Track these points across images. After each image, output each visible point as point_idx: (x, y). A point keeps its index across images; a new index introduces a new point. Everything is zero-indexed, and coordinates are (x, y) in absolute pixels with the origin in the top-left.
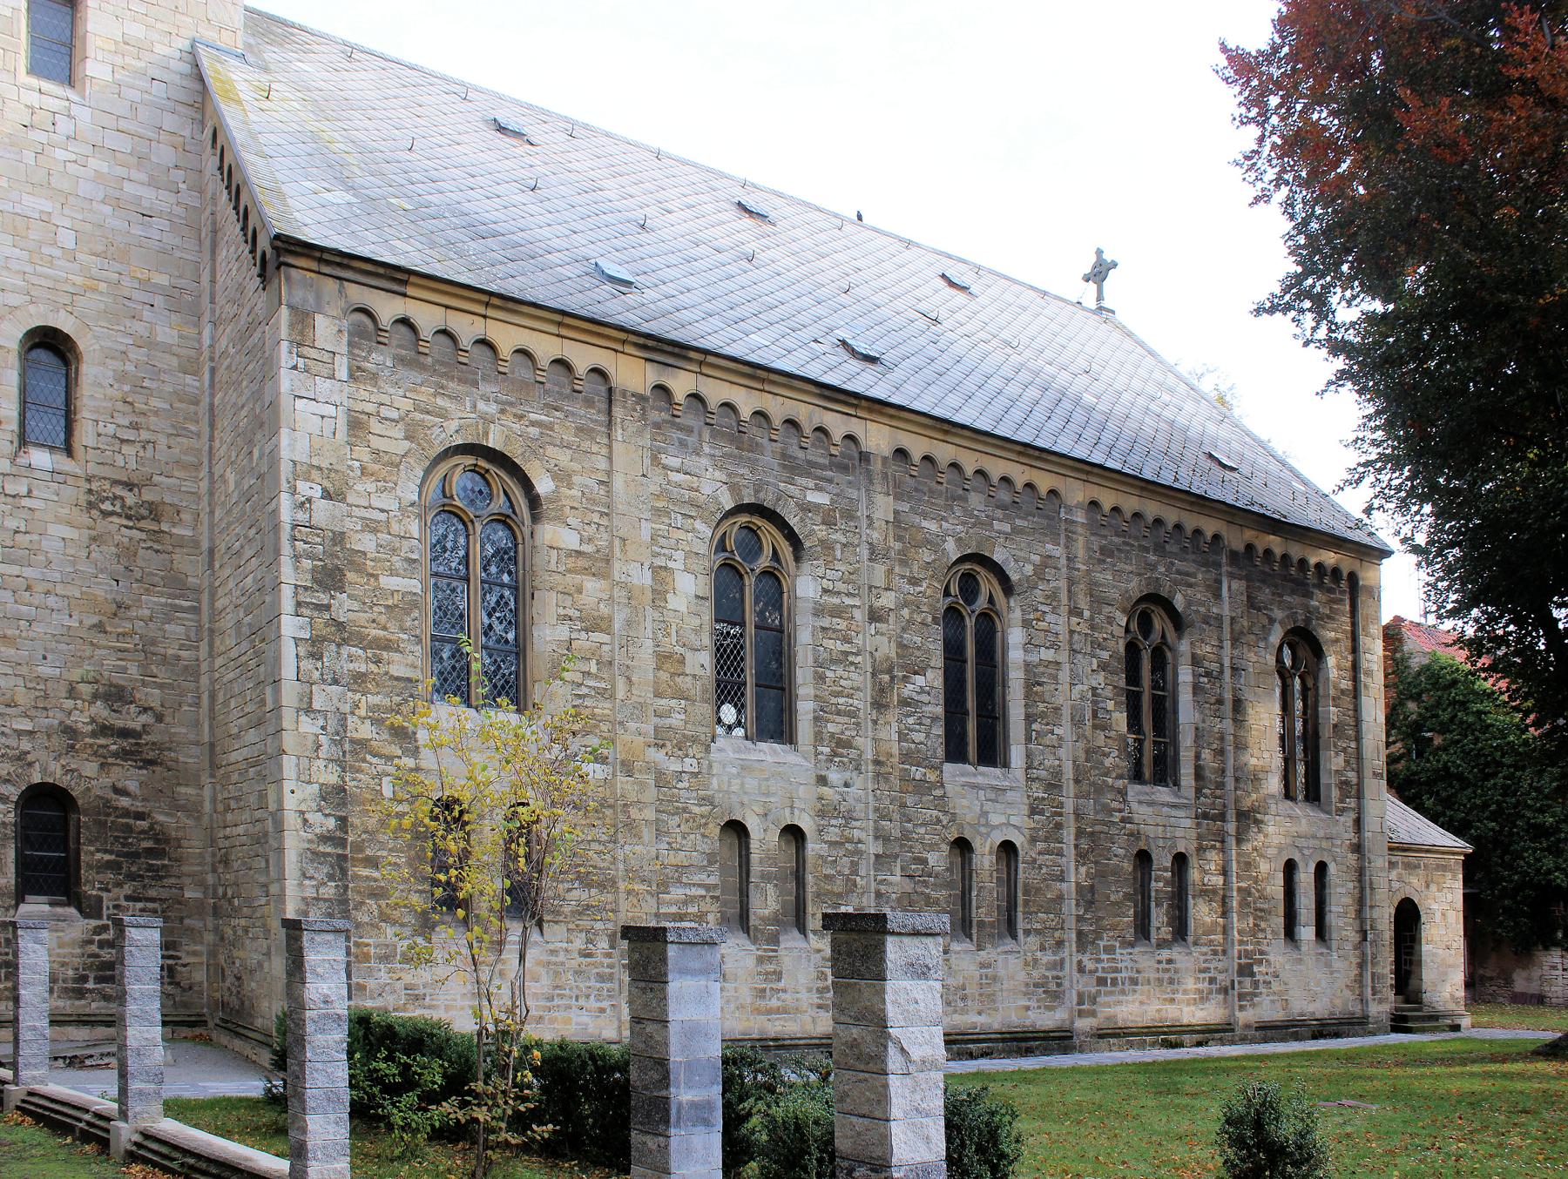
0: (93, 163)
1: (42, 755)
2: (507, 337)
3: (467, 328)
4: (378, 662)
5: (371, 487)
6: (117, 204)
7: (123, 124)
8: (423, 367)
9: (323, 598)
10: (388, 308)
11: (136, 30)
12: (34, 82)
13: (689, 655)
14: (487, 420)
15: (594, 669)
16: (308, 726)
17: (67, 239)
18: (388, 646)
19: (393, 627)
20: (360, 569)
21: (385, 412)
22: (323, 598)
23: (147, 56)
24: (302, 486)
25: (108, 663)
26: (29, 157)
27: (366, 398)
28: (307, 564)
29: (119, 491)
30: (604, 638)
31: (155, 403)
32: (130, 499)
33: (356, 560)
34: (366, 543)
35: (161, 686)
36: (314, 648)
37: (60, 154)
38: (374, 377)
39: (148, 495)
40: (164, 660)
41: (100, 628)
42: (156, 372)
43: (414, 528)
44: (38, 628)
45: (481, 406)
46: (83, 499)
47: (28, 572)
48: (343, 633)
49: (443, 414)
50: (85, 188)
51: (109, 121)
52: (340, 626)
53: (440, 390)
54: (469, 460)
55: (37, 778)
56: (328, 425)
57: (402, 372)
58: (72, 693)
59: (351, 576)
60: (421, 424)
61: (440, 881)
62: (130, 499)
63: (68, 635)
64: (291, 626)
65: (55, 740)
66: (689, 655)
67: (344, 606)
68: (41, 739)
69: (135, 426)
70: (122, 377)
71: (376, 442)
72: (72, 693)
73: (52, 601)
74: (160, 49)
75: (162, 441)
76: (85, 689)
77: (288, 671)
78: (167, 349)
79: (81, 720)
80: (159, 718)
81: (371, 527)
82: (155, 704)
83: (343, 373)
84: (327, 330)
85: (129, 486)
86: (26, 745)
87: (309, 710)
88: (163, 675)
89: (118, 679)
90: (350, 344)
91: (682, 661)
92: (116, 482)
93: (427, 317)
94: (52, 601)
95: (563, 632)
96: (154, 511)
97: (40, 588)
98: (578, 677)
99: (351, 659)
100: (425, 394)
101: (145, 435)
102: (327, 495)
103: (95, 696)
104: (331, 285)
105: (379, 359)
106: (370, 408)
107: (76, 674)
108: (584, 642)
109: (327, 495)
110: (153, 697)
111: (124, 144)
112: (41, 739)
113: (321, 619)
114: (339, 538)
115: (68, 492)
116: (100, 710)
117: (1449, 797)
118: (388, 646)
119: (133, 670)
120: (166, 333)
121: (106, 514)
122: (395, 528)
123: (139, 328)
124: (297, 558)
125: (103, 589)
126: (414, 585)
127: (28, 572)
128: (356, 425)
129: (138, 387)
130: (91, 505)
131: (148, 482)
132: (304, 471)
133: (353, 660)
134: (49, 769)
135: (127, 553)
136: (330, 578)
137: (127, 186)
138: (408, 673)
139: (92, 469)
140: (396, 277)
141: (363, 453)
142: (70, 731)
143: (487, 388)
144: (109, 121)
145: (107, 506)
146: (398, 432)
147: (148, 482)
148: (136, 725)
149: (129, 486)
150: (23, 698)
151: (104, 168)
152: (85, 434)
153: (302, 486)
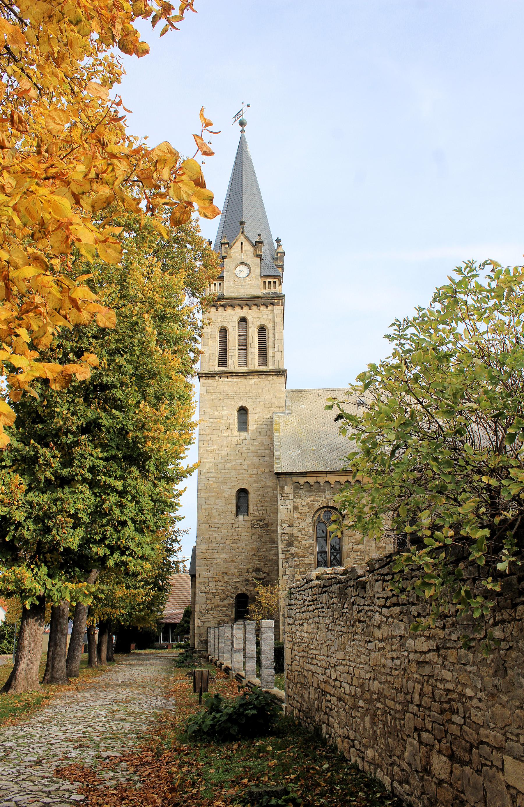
0: (251, 448)
1: (241, 586)
2: (332, 479)
3: (322, 480)
4: (302, 561)
5: (300, 521)
6: (257, 456)
7: (258, 437)
8: (312, 491)
9: (288, 549)
10: (302, 480)
11: (260, 415)
12: (239, 433)
13: (387, 546)
14: (328, 500)
15: (359, 553)
16: (285, 578)
17: (246, 467)
18: (305, 557)
19: (306, 552)
20: (297, 540)
21: (303, 504)
22: (288, 549)
23: (263, 420)
24: (283, 525)
25: (257, 563)
26: (237, 451)
27: (298, 502)
28: (285, 542)
29: (258, 522)
30: (362, 545)
31: (267, 500)
32: (261, 523)
33: (296, 539)
34: (299, 534)
35: (269, 567)
36: (286, 560)
37: (244, 449)
38: (300, 496)
39: (265, 522)
40: (269, 560)
41: (254, 555)
42: (266, 492)
43: (311, 528)
44: (240, 557)
45: (327, 497)
46: (250, 526)
47: (238, 545)
48: (293, 556)
49: (317, 501)
50: (249, 455)
51: (255, 438)
52: (292, 554)
53: (316, 495)
54: (325, 509)
55: (240, 592)
56: (289, 510)
57: (307, 493)
58: (248, 571)
59: (295, 542)
60: (312, 504)
61: (494, 581)
62: (261, 523)
63: (247, 558)
64: (281, 556)
65: (244, 583)
66: (387, 546)
67: (293, 550)
68: (241, 583)
69: (262, 506)
70: (258, 496)
71: (301, 511)
72: (248, 571)
73: (243, 550)
74: (265, 418)
75: (268, 508)
76: (251, 570)
77: (280, 566)
78: (269, 486)
79: (249, 577)
80: (268, 574)
81: (300, 530)
82: (267, 571)
83: (292, 498)
84: (288, 489)
85: (261, 520)
86: (237, 585)
87: (285, 574)
88: (269, 564)
89: (258, 566)
90: (294, 490)
91: (385, 548)
92: (257, 520)
93: (312, 480)
94: (243, 550)
95: (350, 546)
96: (267, 525)
97: (240, 548)
98: (355, 556)
99: (295, 561)
100: (313, 497)
101: (264, 508)
102: (289, 526)
103: (253, 571)
104: (289, 479)
105: (301, 492)
106: (299, 504)
107: (249, 567)
108: (356, 547)
109: (289, 526)
110: (266, 569)
111: (258, 442)
112: (241, 583)
113: (288, 553)
114: (292, 535)
115: (247, 525)
116: (254, 574)
117: (474, 584)
118: (305, 557)
119: (262, 564)
120: (269, 483)
121: (255, 528)
122: (306, 529)
123: (263, 483)
124: (282, 541)
125: (255, 546)
126: (312, 542)
127: (238, 545)
128: (296, 508)
129: (263, 497)
130: (252, 527)
131: (266, 518)
132: (284, 522)
133: (297, 561)
134: (242, 589)
135: (261, 536)
136: (290, 544)
137: (259, 451)
138: (310, 562)
139: (252, 518)
140: (304, 474)
141: (298, 514)
142: (247, 580)
143: (328, 492)
144: (255, 438)
145: (256, 526)
146: (306, 507)
147: (266, 518)
148: (262, 577)
149: (261, 520)
150: (237, 574)
151: (254, 449)
152: (251, 511)
153: (283, 525)
